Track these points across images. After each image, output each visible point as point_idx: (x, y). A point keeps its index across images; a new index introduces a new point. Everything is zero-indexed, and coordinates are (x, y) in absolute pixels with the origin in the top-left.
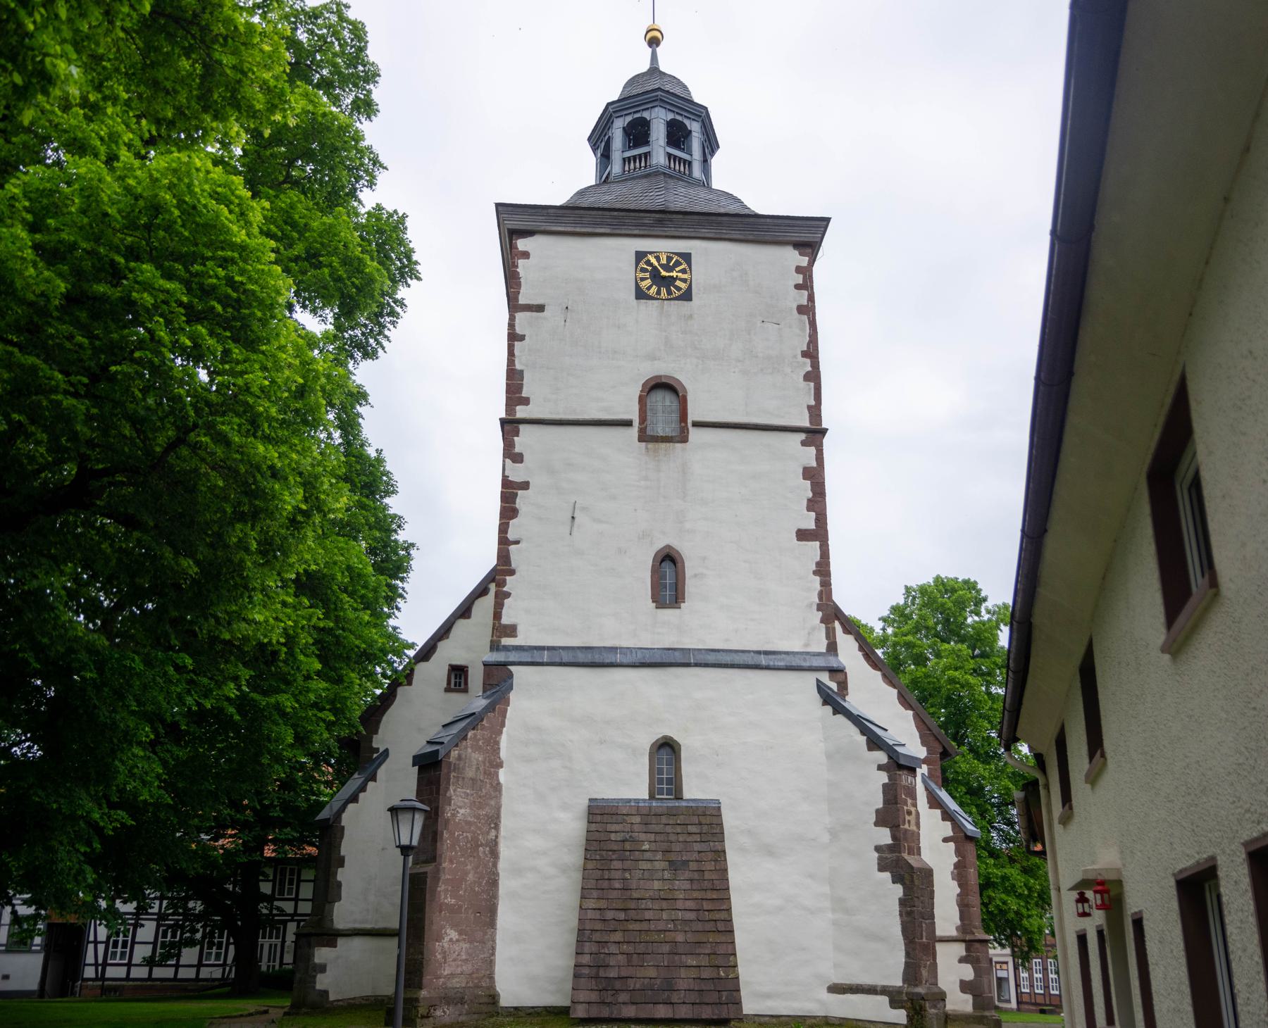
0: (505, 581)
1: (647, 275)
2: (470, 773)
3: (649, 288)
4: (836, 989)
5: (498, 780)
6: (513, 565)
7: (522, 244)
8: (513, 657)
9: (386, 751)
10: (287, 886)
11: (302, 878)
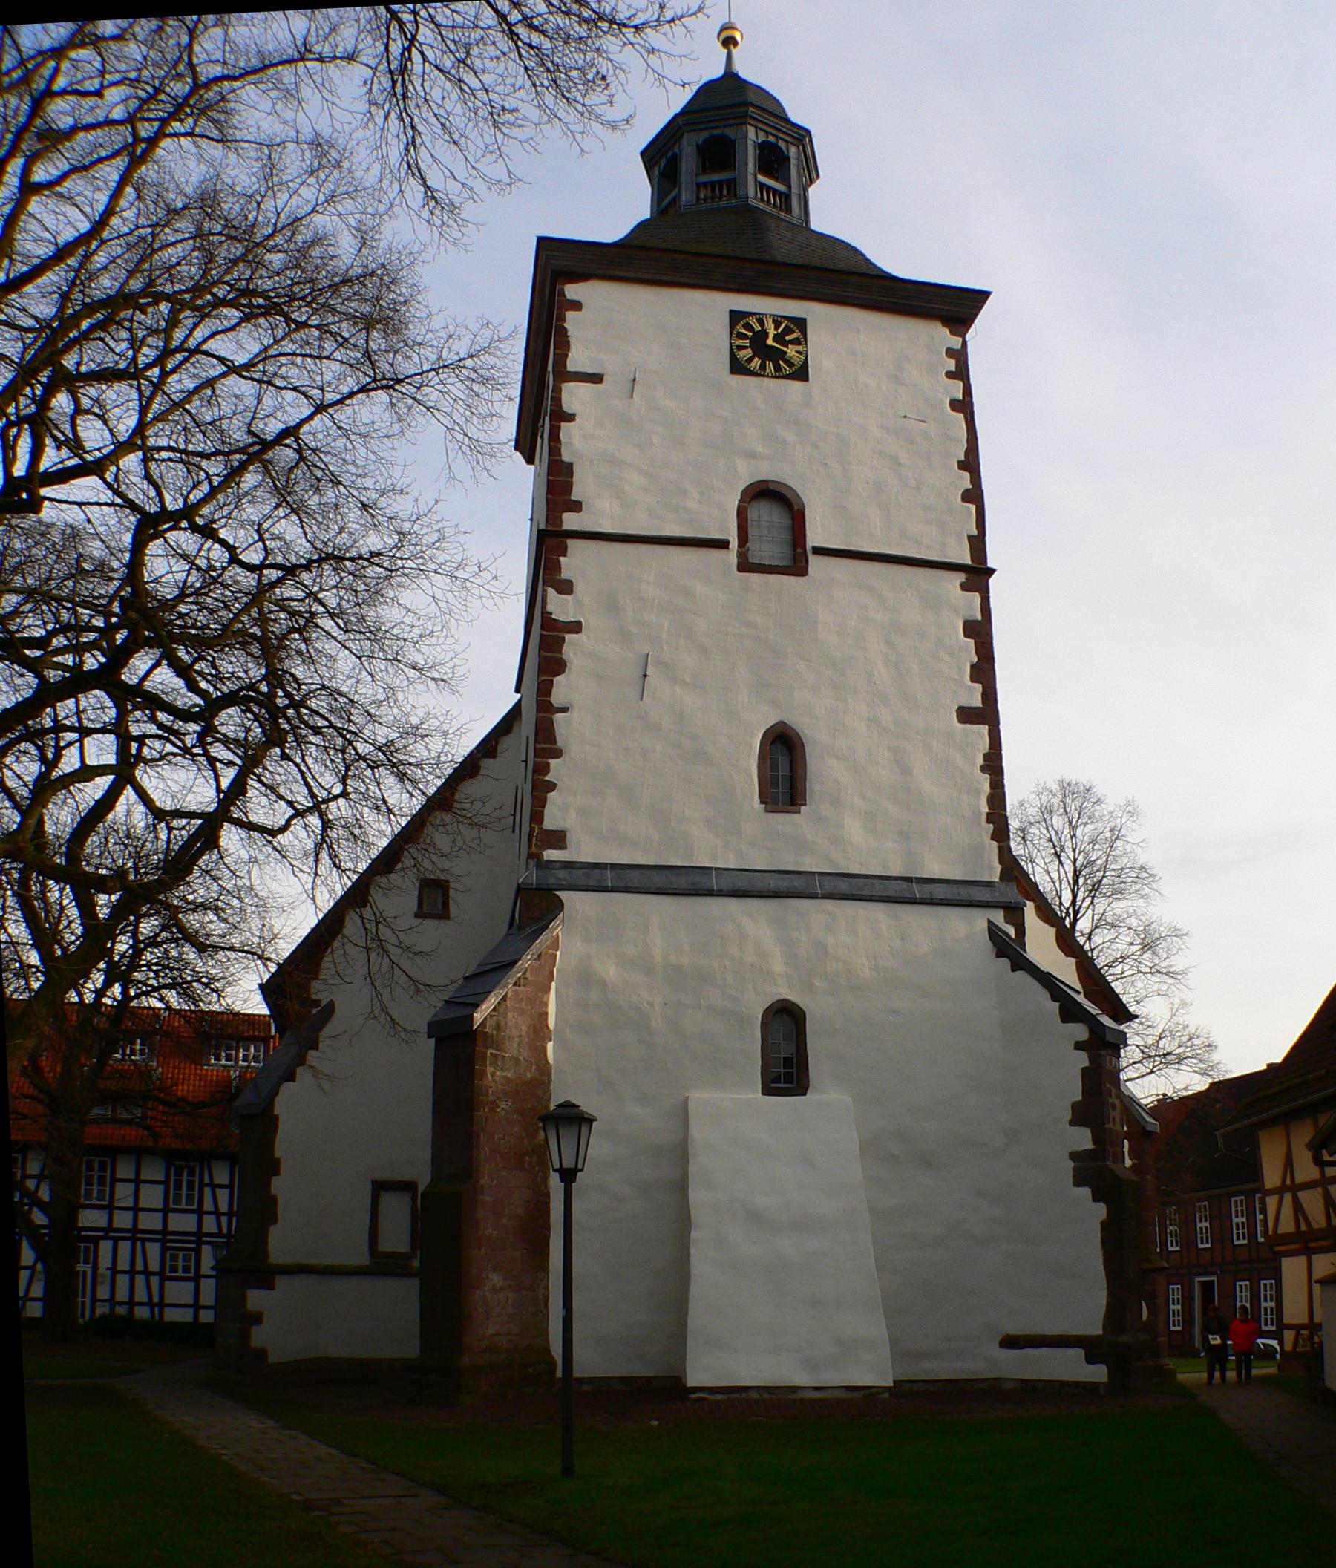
1: (747, 343)
3: (750, 360)
4: (1010, 1342)
6: (560, 743)
7: (572, 291)
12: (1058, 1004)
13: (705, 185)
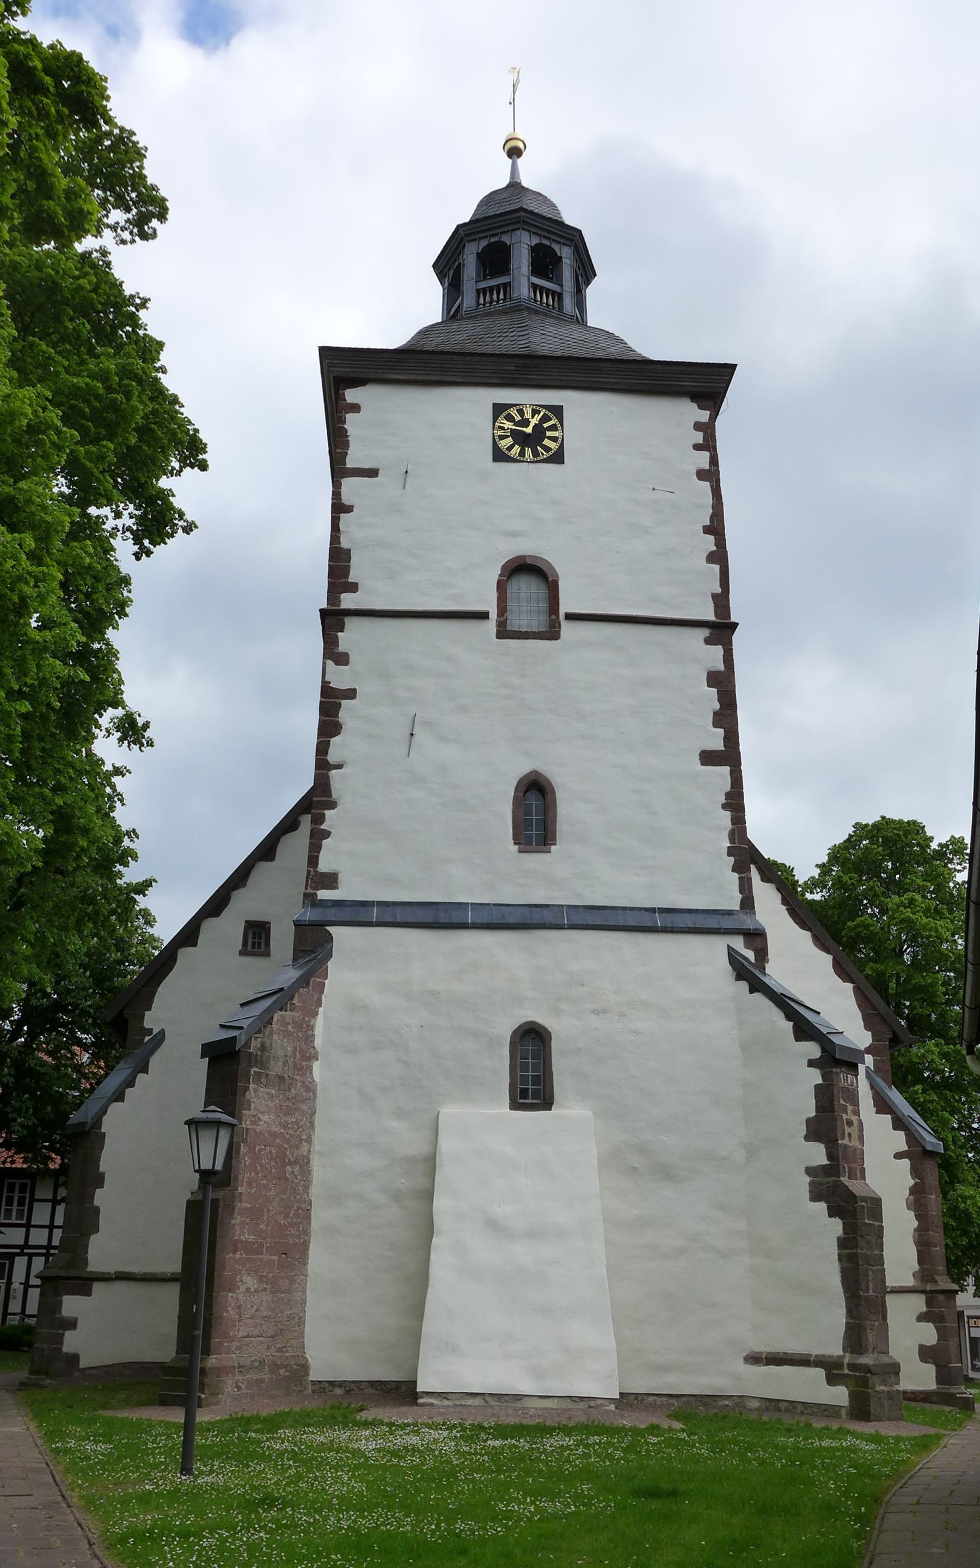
0: (323, 816)
2: (276, 1068)
3: (510, 448)
4: (754, 1359)
5: (312, 1078)
6: (335, 795)
7: (351, 395)
8: (331, 914)
9: (162, 1033)
10: (3, 1207)
11: (36, 1197)
12: (792, 1023)
13: (484, 290)
